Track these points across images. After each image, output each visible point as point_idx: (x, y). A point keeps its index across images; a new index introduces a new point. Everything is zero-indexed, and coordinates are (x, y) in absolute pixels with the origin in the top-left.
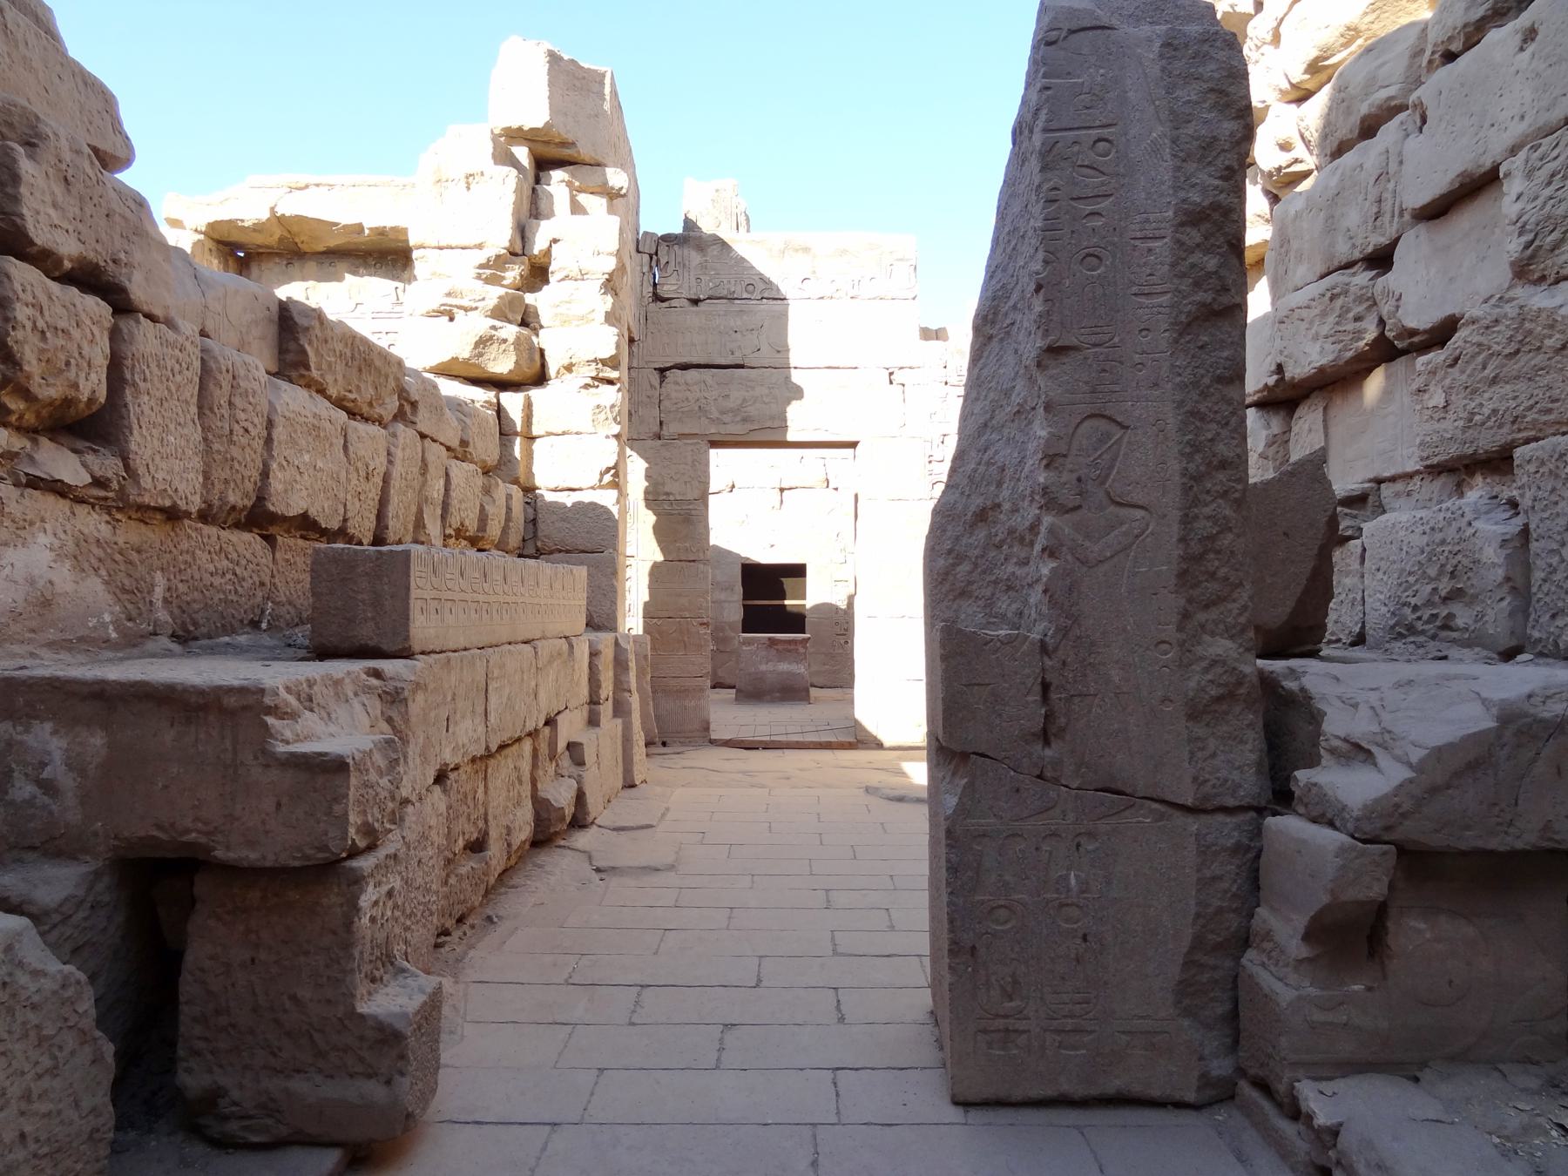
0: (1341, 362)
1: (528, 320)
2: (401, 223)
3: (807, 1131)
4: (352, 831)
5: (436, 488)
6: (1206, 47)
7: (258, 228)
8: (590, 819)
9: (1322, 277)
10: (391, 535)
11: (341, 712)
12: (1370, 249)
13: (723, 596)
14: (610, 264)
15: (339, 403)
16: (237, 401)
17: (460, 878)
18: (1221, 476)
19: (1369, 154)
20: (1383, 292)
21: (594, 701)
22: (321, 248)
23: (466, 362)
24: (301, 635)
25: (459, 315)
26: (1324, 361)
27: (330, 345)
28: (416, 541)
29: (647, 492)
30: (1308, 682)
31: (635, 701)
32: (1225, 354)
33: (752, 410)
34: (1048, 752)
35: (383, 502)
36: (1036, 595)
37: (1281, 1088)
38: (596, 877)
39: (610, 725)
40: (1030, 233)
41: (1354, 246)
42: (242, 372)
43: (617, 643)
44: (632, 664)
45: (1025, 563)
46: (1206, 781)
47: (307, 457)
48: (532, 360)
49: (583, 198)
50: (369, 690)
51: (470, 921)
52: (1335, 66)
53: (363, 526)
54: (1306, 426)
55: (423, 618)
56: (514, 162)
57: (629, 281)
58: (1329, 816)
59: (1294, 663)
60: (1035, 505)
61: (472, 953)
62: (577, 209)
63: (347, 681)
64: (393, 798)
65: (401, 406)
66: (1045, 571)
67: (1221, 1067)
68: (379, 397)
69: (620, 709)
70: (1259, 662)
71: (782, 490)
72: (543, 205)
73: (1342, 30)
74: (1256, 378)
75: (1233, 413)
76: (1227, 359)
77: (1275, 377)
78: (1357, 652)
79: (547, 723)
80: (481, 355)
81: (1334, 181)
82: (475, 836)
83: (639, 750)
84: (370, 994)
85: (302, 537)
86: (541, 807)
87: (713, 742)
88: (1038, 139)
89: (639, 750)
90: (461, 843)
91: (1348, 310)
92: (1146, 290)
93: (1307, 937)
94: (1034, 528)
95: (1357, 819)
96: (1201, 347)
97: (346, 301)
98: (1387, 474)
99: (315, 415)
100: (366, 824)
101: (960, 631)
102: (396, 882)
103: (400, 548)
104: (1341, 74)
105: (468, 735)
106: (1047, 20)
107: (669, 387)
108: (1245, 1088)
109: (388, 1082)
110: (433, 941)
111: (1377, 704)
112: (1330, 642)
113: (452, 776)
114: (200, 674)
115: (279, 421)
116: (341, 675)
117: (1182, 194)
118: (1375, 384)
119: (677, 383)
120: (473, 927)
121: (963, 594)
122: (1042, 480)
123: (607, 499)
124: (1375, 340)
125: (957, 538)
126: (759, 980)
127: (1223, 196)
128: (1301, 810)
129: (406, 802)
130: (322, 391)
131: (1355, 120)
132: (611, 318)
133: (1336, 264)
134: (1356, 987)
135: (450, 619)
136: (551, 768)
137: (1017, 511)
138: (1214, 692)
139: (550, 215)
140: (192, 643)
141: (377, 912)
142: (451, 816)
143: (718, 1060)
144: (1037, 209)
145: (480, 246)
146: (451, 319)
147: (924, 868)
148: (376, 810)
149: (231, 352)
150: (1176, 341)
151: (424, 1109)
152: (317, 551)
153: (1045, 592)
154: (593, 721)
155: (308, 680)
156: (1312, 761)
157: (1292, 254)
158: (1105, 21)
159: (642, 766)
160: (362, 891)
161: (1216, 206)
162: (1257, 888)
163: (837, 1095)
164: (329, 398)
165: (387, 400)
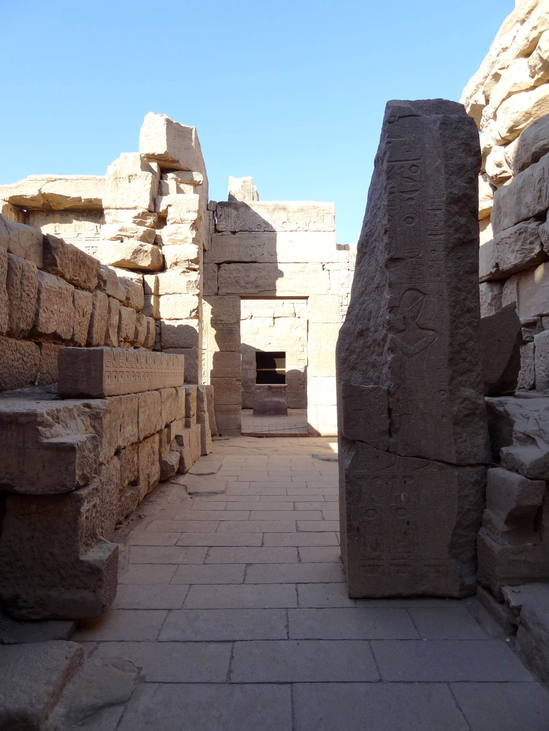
0: (524, 262)
1: (157, 242)
2: (99, 197)
3: (284, 612)
4: (77, 478)
5: (115, 319)
6: (460, 125)
7: (33, 199)
8: (186, 470)
9: (515, 224)
10: (95, 342)
11: (72, 424)
12: (536, 212)
13: (247, 367)
14: (194, 216)
15: (70, 282)
16: (25, 282)
17: (127, 498)
18: (468, 315)
19: (535, 170)
20: (542, 231)
21: (188, 416)
22: (62, 208)
23: (129, 261)
24: (54, 388)
25: (126, 240)
26: (517, 262)
27: (66, 256)
28: (106, 345)
29: (212, 320)
30: (507, 407)
31: (206, 415)
32: (470, 261)
33: (260, 282)
34: (391, 440)
35: (91, 326)
36: (385, 370)
37: (496, 589)
38: (188, 497)
39: (195, 427)
40: (382, 207)
41: (529, 211)
42: (26, 269)
43: (198, 389)
44: (205, 399)
45: (380, 354)
46: (461, 453)
47: (56, 307)
48: (159, 260)
49: (182, 186)
50: (84, 413)
51: (131, 517)
52: (521, 130)
53: (82, 338)
54: (509, 291)
55: (109, 380)
56: (150, 170)
57: (204, 223)
58: (516, 467)
59: (502, 399)
60: (384, 329)
61: (132, 532)
62: (179, 191)
63: (75, 409)
64: (96, 463)
65: (99, 282)
66: (389, 359)
67: (469, 580)
68: (89, 278)
69: (200, 420)
70: (486, 398)
71: (274, 318)
72: (164, 189)
73: (524, 114)
74: (485, 268)
75: (473, 288)
76: (470, 263)
77: (495, 269)
78: (532, 393)
79: (166, 427)
80: (135, 258)
81: (520, 182)
82: (133, 479)
83: (209, 438)
84: (86, 551)
85: (54, 343)
86: (164, 465)
87: (243, 434)
88: (385, 165)
89: (209, 438)
90: (127, 482)
91: (527, 239)
92: (434, 232)
93: (507, 522)
94: (384, 339)
95: (528, 469)
96: (459, 258)
97: (73, 234)
98: (545, 313)
99: (60, 288)
100: (83, 474)
101: (351, 385)
102: (97, 501)
103: (98, 348)
104: (523, 134)
105: (130, 433)
106: (389, 112)
107: (222, 272)
108: (480, 590)
109: (94, 591)
110: (114, 527)
111: (537, 417)
112: (520, 388)
113: (123, 451)
114: (8, 407)
115: (43, 290)
116: (72, 407)
117: (449, 190)
118: (540, 272)
119: (225, 270)
120: (132, 520)
121: (353, 369)
122: (388, 318)
123: (194, 323)
124: (539, 252)
125: (351, 343)
126: (263, 544)
127: (468, 191)
128: (504, 465)
129: (101, 464)
130: (63, 276)
131: (529, 154)
132: (195, 241)
133: (521, 218)
134: (529, 544)
135: (121, 380)
136: (168, 447)
137: (377, 331)
138: (465, 412)
139: (167, 194)
140: (4, 392)
141: (88, 514)
142: (122, 469)
143: (244, 580)
144: (385, 197)
145: (135, 208)
146: (122, 242)
147: (337, 492)
148: (88, 468)
149: (21, 260)
150: (447, 256)
151: (111, 604)
152: (61, 350)
153: (389, 368)
154: (187, 425)
155: (57, 410)
156: (509, 443)
157: (502, 214)
158: (415, 113)
159: (210, 445)
160: (82, 505)
161: (465, 195)
162: (486, 500)
163: (298, 595)
164: (66, 279)
165: (93, 280)
